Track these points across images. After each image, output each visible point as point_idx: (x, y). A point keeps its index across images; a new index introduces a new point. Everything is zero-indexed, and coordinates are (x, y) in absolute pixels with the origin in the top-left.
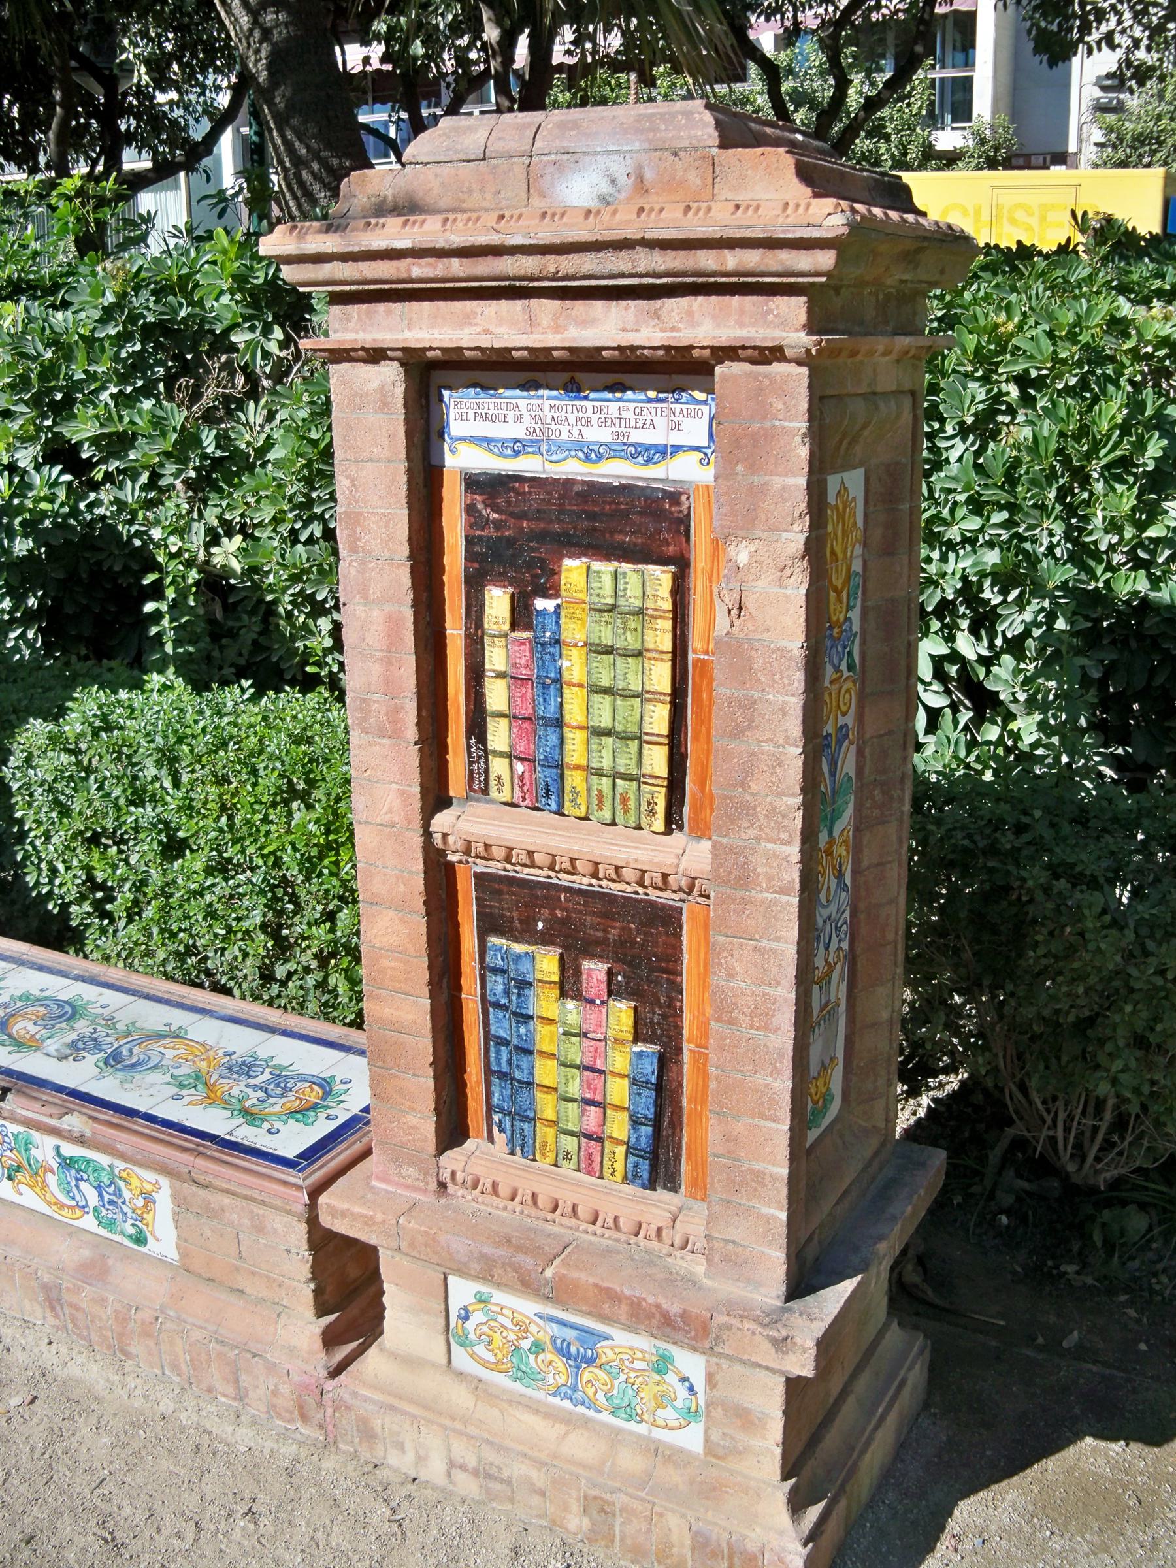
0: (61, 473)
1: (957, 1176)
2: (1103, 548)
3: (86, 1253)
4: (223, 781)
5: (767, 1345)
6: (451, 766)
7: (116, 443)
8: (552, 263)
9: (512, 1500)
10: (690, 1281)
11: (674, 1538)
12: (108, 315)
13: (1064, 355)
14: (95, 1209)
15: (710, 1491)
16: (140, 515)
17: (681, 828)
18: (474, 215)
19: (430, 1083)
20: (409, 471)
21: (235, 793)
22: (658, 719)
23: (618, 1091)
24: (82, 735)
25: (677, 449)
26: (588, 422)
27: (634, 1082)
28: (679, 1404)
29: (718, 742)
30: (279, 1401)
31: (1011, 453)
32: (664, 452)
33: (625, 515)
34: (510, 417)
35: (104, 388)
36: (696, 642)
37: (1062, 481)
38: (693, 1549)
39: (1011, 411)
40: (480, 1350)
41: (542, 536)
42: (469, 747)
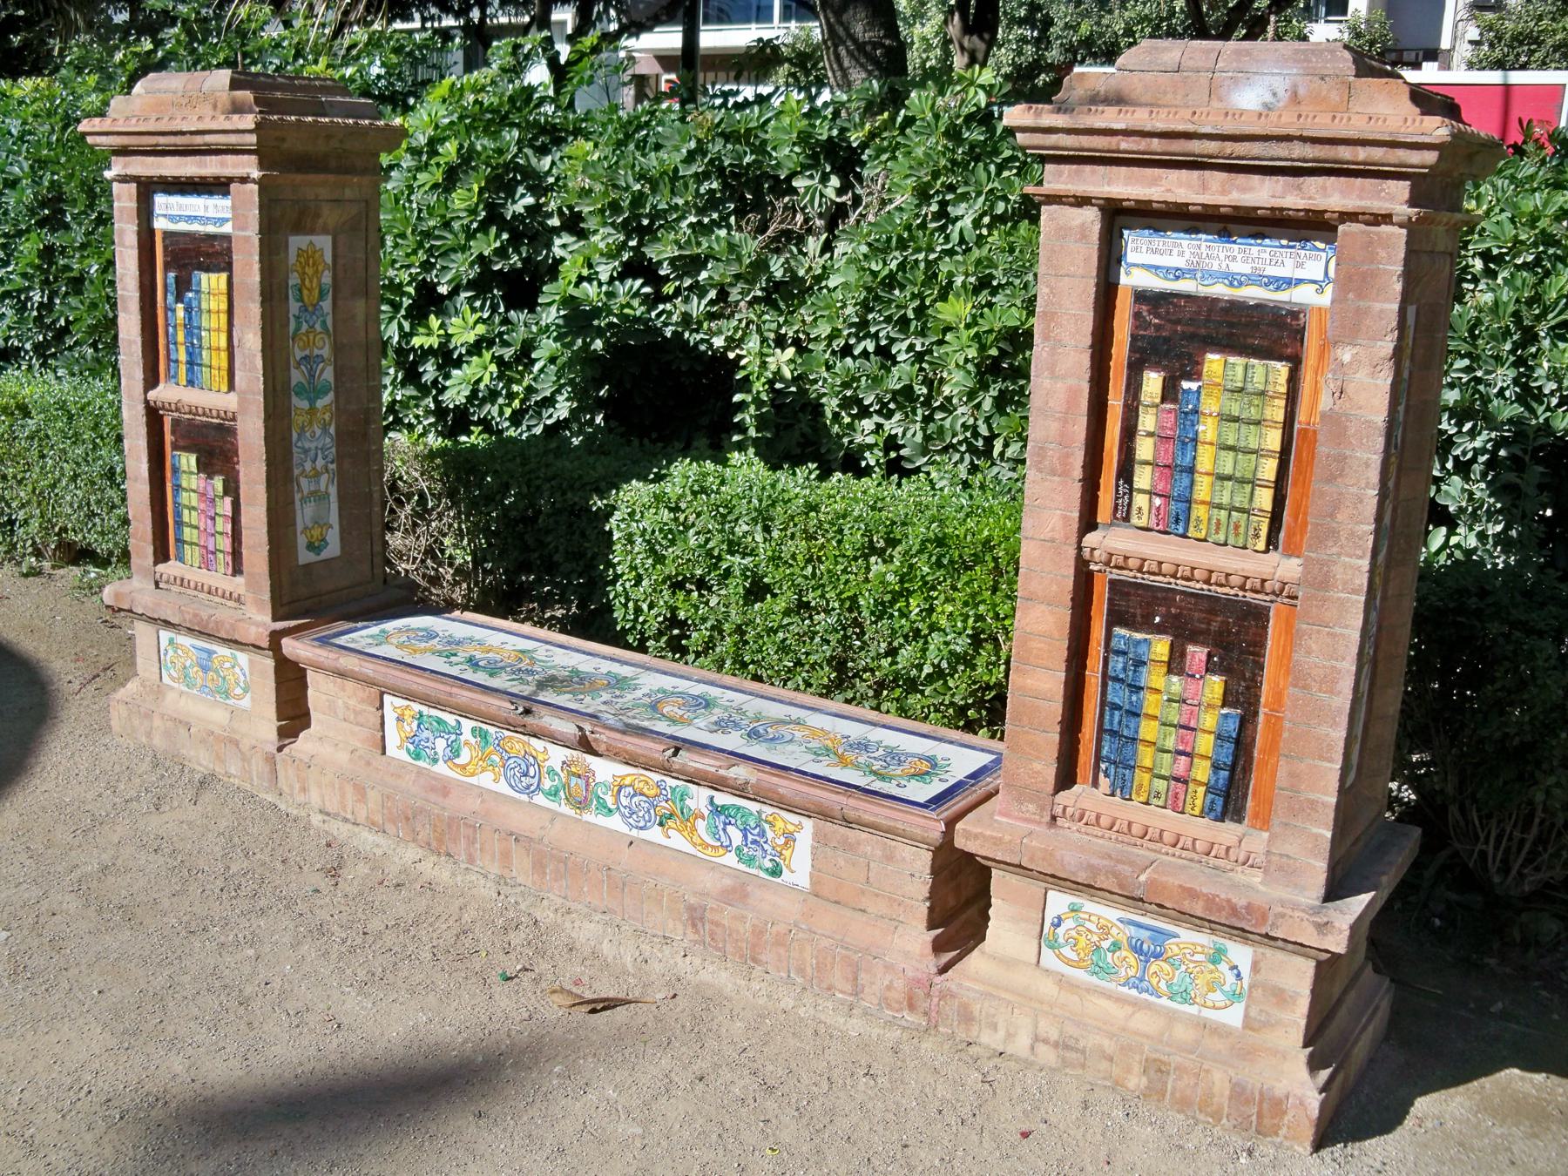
0: (642, 285)
1: (1429, 847)
2: (1547, 391)
3: (728, 882)
4: (810, 537)
5: (1311, 929)
6: (1101, 500)
7: (690, 264)
8: (1229, 147)
9: (1083, 1066)
10: (1249, 887)
11: (1216, 1090)
12: (690, 158)
13: (1523, 237)
14: (738, 848)
15: (1247, 1053)
16: (705, 325)
17: (1276, 548)
18: (1173, 110)
19: (1057, 737)
20: (1097, 285)
21: (823, 547)
22: (1269, 469)
23: (1205, 744)
24: (683, 496)
25: (1300, 281)
26: (1234, 258)
27: (1219, 737)
28: (1227, 988)
29: (1316, 485)
30: (893, 995)
31: (1473, 313)
32: (1290, 283)
33: (1257, 325)
34: (1175, 251)
35: (683, 217)
36: (1301, 417)
37: (1515, 337)
38: (1230, 1098)
39: (1475, 280)
40: (1067, 951)
41: (1192, 337)
42: (1117, 486)
